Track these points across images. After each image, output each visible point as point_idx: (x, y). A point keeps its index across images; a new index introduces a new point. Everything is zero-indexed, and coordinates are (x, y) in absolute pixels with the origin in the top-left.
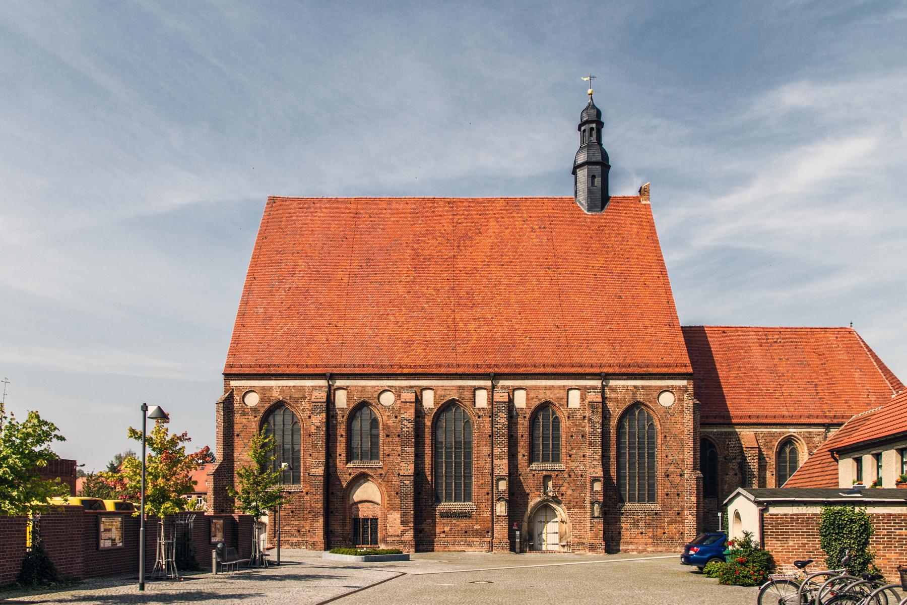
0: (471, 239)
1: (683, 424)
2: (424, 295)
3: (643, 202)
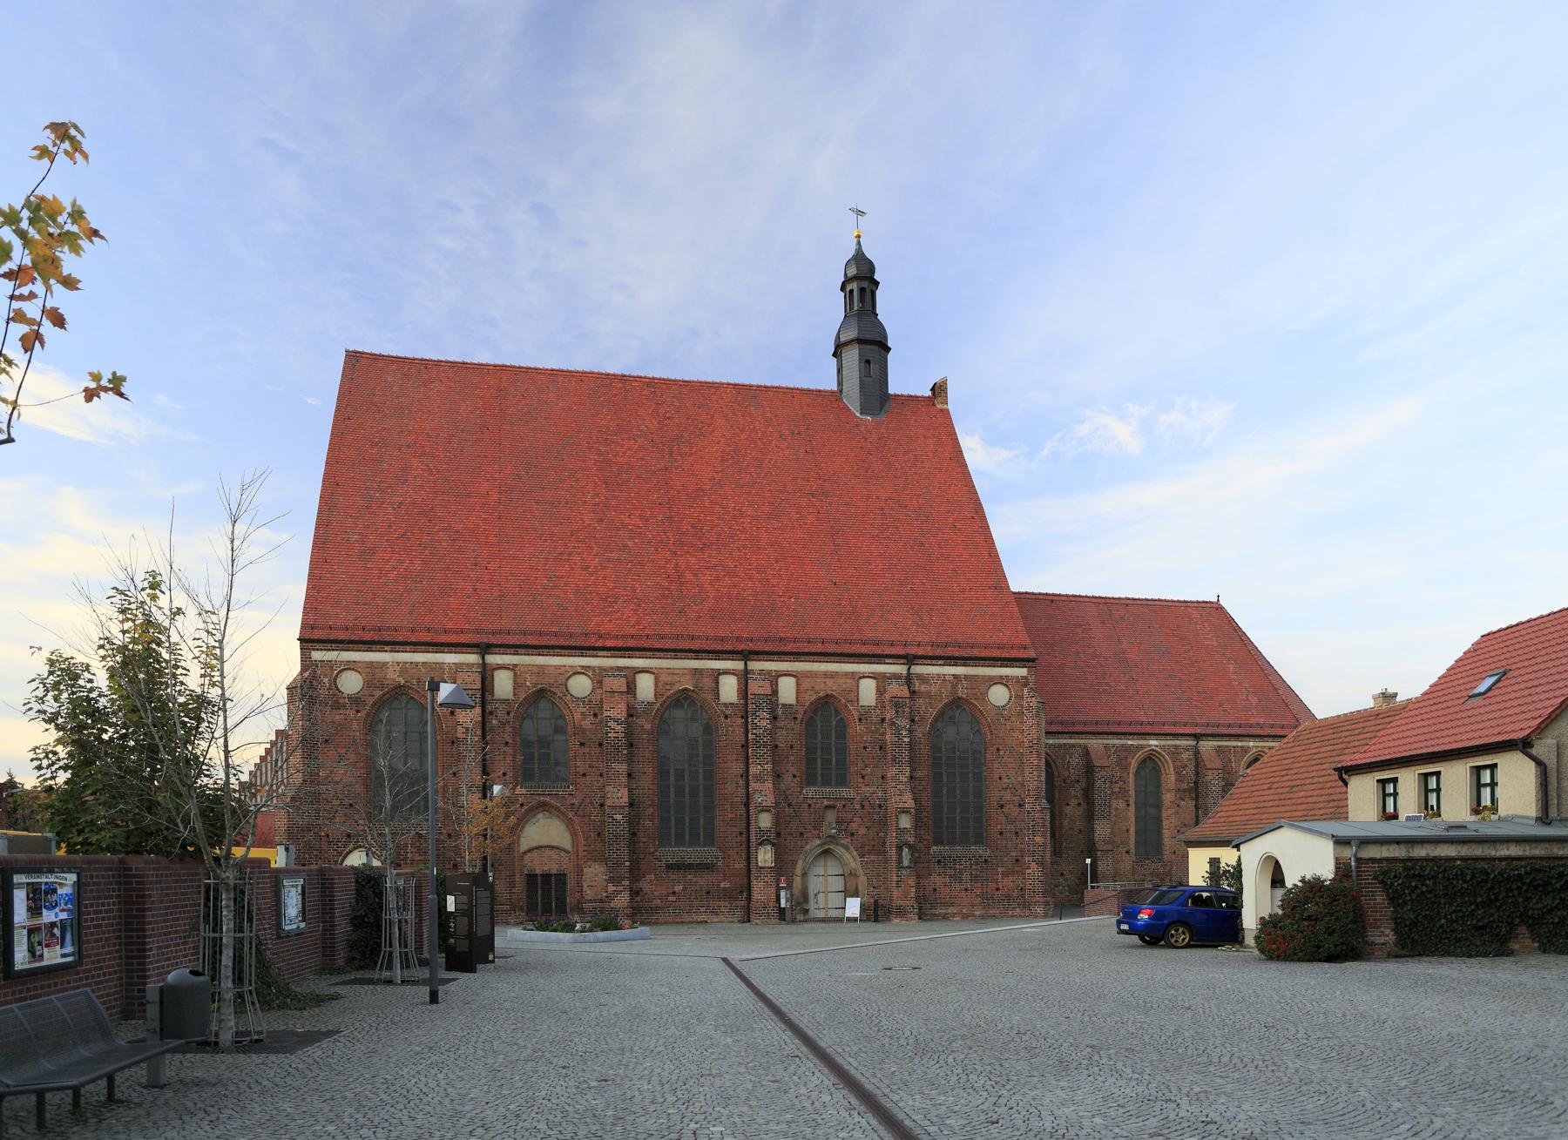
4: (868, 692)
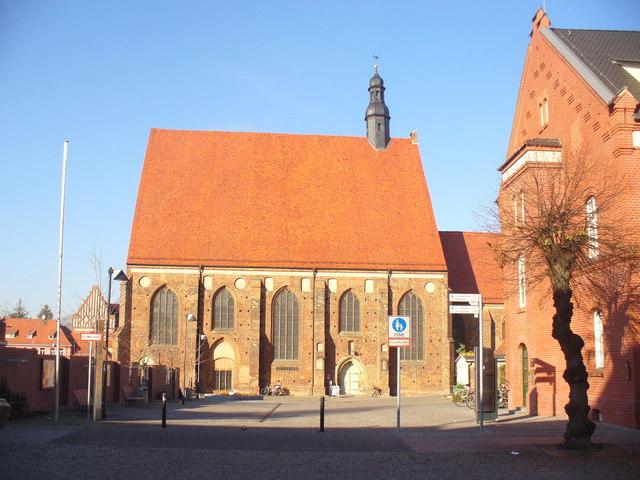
0: (295, 165)
2: (264, 207)
4: (370, 287)
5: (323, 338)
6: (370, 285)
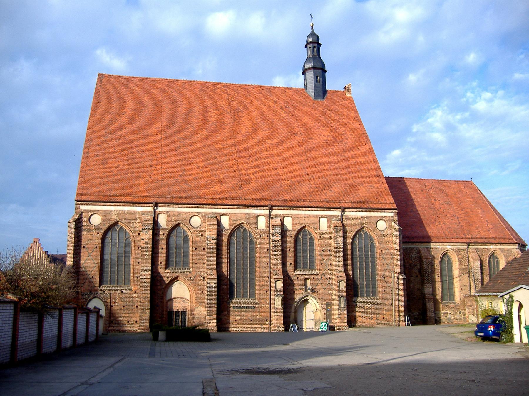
1: (392, 243)
2: (215, 148)
3: (348, 95)
4: (324, 224)
5: (281, 275)
6: (324, 223)
